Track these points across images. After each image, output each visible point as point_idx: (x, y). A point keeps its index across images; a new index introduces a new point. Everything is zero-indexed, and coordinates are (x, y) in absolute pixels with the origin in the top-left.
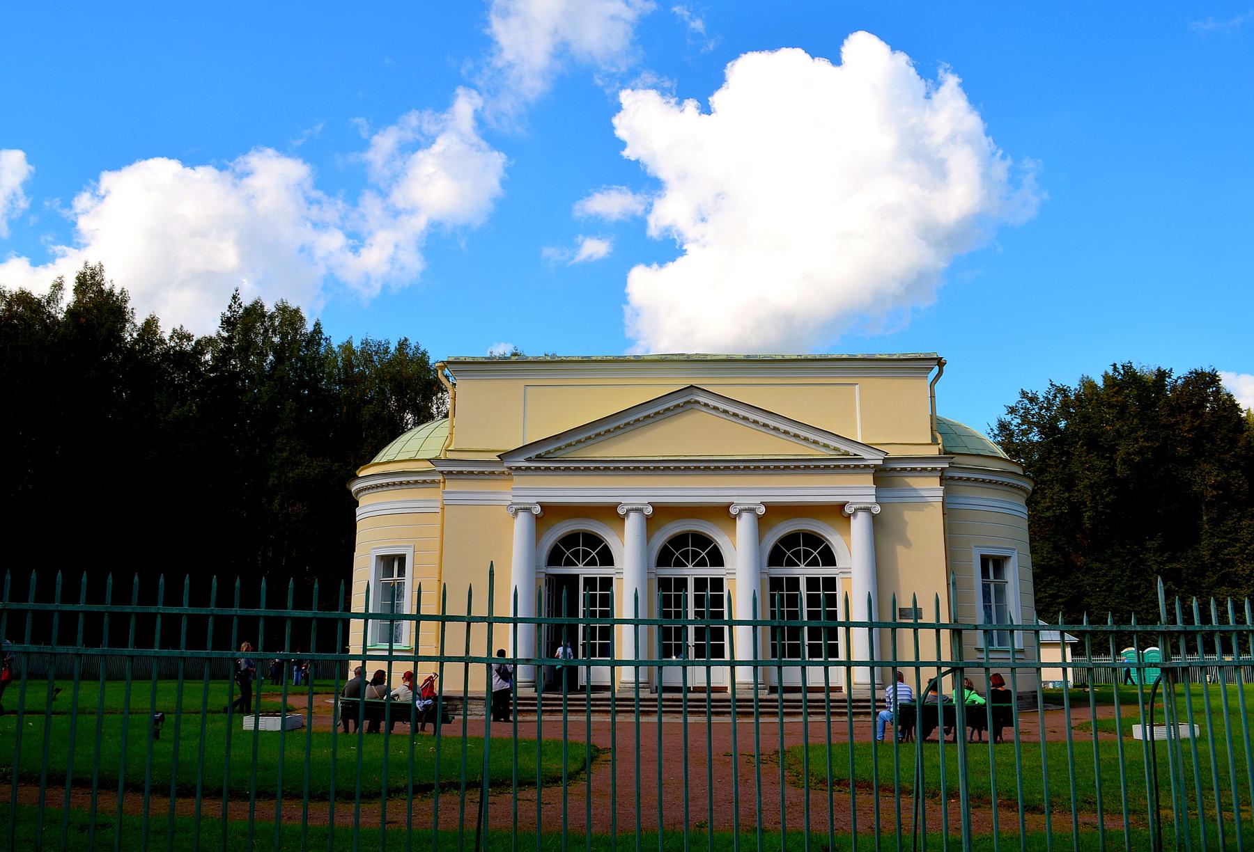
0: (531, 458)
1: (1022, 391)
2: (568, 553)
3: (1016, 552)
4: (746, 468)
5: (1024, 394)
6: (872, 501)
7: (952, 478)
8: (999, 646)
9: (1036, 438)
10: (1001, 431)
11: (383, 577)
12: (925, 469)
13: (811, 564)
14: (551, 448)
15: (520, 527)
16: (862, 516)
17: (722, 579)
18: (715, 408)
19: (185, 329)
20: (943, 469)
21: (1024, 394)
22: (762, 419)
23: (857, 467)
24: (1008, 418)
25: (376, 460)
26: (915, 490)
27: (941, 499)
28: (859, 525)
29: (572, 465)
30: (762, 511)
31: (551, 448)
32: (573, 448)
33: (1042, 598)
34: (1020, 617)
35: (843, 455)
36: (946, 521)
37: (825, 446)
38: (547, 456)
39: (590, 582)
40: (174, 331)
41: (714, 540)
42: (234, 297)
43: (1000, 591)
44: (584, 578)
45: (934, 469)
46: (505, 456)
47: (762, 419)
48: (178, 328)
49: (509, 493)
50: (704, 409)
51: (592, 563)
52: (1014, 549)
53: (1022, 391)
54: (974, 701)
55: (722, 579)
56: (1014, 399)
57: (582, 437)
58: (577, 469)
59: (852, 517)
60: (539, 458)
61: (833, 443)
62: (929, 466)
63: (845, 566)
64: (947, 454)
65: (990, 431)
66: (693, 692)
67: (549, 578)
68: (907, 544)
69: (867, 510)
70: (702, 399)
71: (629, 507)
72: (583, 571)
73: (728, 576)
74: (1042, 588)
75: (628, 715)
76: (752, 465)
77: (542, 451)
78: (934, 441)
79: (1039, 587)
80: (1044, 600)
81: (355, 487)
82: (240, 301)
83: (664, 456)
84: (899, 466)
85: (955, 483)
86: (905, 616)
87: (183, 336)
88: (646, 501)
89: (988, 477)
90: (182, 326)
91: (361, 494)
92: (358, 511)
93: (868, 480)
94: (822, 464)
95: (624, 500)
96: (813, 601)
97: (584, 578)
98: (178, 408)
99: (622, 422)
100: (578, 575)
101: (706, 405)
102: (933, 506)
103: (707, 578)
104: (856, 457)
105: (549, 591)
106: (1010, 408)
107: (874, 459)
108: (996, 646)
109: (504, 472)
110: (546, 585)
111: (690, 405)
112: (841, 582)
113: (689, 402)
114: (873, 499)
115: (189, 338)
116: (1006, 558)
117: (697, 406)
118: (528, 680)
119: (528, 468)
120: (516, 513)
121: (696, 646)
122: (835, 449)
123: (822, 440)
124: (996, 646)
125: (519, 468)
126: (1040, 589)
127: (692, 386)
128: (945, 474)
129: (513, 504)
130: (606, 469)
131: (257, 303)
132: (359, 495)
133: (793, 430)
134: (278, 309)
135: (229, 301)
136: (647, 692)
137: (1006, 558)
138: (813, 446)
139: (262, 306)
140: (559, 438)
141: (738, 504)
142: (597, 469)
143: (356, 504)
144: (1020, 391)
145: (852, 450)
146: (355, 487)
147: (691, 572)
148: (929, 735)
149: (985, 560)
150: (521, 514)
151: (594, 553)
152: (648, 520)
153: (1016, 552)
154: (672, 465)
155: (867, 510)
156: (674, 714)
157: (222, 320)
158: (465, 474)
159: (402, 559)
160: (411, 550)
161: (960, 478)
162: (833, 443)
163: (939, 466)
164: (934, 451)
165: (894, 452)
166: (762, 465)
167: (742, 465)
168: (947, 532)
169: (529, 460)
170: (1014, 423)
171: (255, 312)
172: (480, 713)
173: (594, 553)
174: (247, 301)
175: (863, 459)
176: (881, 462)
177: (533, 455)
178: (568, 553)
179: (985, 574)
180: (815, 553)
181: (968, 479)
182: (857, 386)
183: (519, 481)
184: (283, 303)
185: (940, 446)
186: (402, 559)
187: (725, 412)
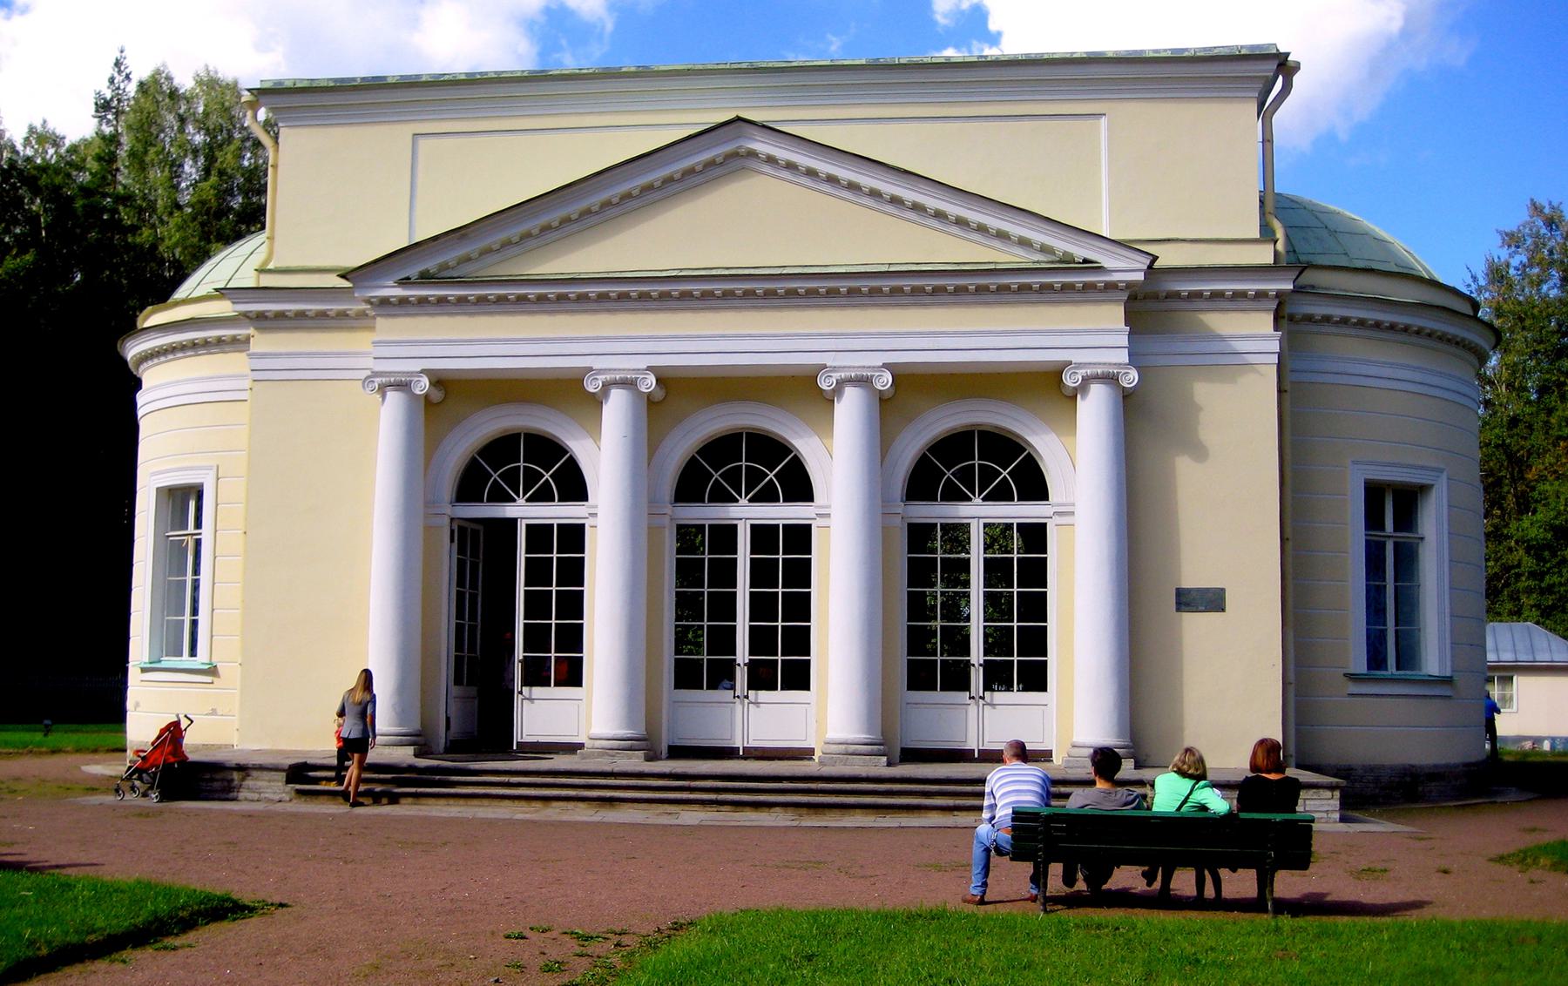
0: (408, 278)
1: (1534, 204)
2: (716, 476)
3: (1444, 477)
4: (852, 292)
5: (1536, 208)
6: (1121, 361)
7: (1309, 319)
8: (1398, 669)
9: (1554, 293)
10: (1491, 282)
11: (172, 530)
12: (1241, 295)
13: (993, 497)
14: (450, 256)
15: (389, 416)
16: (1098, 393)
17: (810, 525)
18: (791, 166)
19: (51, 126)
20: (1280, 295)
21: (1536, 208)
22: (889, 187)
23: (1088, 287)
24: (1504, 254)
25: (181, 293)
26: (1221, 338)
27: (1275, 359)
28: (1094, 410)
29: (532, 291)
30: (885, 381)
31: (450, 256)
32: (496, 257)
33: (1553, 585)
34: (1447, 610)
35: (1061, 262)
36: (1287, 405)
37: (1024, 243)
38: (441, 275)
39: (539, 535)
40: (32, 130)
41: (794, 446)
42: (118, 64)
43: (1407, 558)
44: (527, 525)
45: (1261, 295)
46: (357, 275)
47: (889, 187)
48: (38, 125)
49: (364, 354)
50: (766, 168)
51: (543, 496)
52: (1442, 471)
53: (1534, 204)
54: (1203, 808)
55: (810, 525)
56: (1517, 218)
57: (514, 232)
58: (502, 300)
59: (1079, 396)
60: (426, 278)
61: (1038, 236)
62: (1251, 287)
63: (1064, 501)
64: (1293, 263)
65: (1470, 281)
66: (745, 758)
67: (460, 528)
68: (1199, 452)
69: (1110, 379)
70: (763, 146)
71: (608, 377)
72: (524, 511)
73: (1057, 520)
74: (1554, 566)
75: (571, 805)
76: (865, 285)
77: (430, 265)
78: (1267, 234)
79: (1548, 565)
80: (1556, 590)
81: (133, 350)
82: (128, 71)
83: (661, 271)
84: (1186, 287)
85: (1315, 328)
86: (1188, 605)
87: (42, 137)
88: (879, 360)
89: (1387, 317)
90: (45, 122)
91: (145, 365)
92: (141, 398)
93: (1112, 316)
94: (1014, 281)
95: (1075, 356)
96: (762, 572)
97: (527, 525)
98: (15, 257)
99: (594, 200)
100: (515, 520)
101: (771, 160)
102: (1258, 372)
103: (778, 525)
104: (1088, 265)
105: (461, 551)
106: (1507, 234)
107: (1127, 269)
108: (1391, 667)
109: (364, 311)
110: (452, 540)
111: (737, 163)
112: (1055, 531)
113: (735, 155)
114: (1123, 356)
115: (56, 141)
116: (1433, 485)
117: (752, 164)
118: (403, 730)
119: (403, 301)
120: (382, 390)
121: (987, 666)
122: (1044, 249)
123: (1016, 229)
124: (1391, 667)
125: (384, 302)
126: (1549, 569)
127: (739, 119)
128: (1288, 310)
129: (376, 374)
130: (562, 298)
131: (158, 72)
132: (142, 368)
133: (954, 209)
134: (200, 82)
135: (110, 70)
136: (638, 757)
137: (1423, 489)
138: (997, 243)
139: (169, 79)
140: (463, 236)
141: (835, 369)
142: (542, 299)
143: (137, 384)
144: (1529, 202)
145: (1080, 251)
146: (133, 350)
147: (745, 514)
148: (1105, 883)
149: (1374, 493)
150: (393, 396)
151: (547, 476)
152: (651, 402)
153: (1444, 477)
154: (696, 288)
155: (1110, 379)
156: (666, 806)
157: (96, 104)
158: (291, 318)
159: (198, 492)
160: (212, 474)
161: (1327, 319)
162: (1038, 236)
163: (1273, 286)
164: (1264, 255)
165: (1169, 257)
166: (886, 284)
167: (843, 285)
168: (1287, 431)
169: (405, 282)
170: (1515, 262)
171: (157, 90)
172: (277, 797)
173: (547, 476)
174: (141, 70)
175: (1100, 269)
176: (1140, 277)
177: (413, 271)
178: (744, 463)
179: (1373, 519)
180: (1005, 473)
181: (1345, 321)
182: (1103, 121)
183: (390, 328)
184: (208, 72)
185: (1280, 246)
186: (198, 492)
187: (832, 180)
